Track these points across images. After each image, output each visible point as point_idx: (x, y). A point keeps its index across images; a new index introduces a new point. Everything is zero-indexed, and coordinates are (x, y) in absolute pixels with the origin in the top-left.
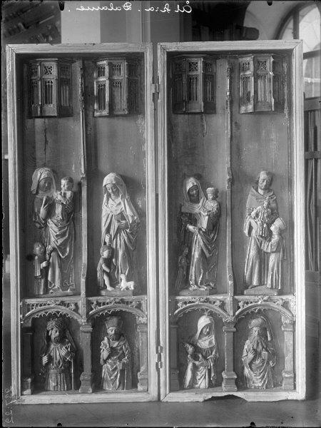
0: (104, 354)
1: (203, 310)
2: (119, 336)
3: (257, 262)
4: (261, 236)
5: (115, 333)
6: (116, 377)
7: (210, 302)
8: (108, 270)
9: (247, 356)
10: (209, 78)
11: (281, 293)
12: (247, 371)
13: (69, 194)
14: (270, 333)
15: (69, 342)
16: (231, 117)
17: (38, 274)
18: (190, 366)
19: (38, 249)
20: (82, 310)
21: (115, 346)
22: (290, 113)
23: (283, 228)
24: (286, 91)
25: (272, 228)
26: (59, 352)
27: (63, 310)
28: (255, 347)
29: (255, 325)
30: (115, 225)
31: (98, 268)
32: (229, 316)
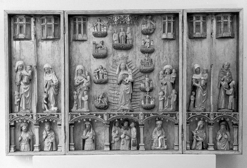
8: (46, 102)
17: (16, 103)
26: (25, 136)
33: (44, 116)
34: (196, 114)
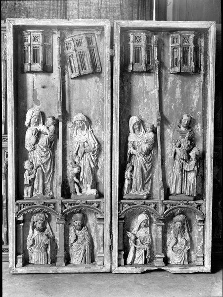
7: (46, 205)
9: (171, 240)
33: (74, 204)
34: (35, 204)
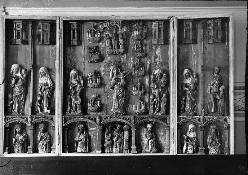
0: (39, 138)
1: (191, 121)
2: (44, 131)
3: (214, 103)
4: (215, 92)
5: (43, 130)
6: (44, 147)
7: (22, 118)
8: (40, 105)
9: (209, 140)
10: (195, 29)
11: (223, 115)
12: (209, 147)
13: (24, 75)
14: (219, 132)
15: (24, 134)
16: (203, 45)
17: (9, 105)
18: (185, 144)
19: (10, 96)
20: (29, 120)
21: (43, 135)
22: (228, 43)
23: (224, 89)
24: (226, 35)
25: (220, 89)
26: (19, 137)
27: (21, 120)
28: (212, 137)
29: (212, 128)
30: (44, 87)
31: (36, 104)
32: (201, 124)
